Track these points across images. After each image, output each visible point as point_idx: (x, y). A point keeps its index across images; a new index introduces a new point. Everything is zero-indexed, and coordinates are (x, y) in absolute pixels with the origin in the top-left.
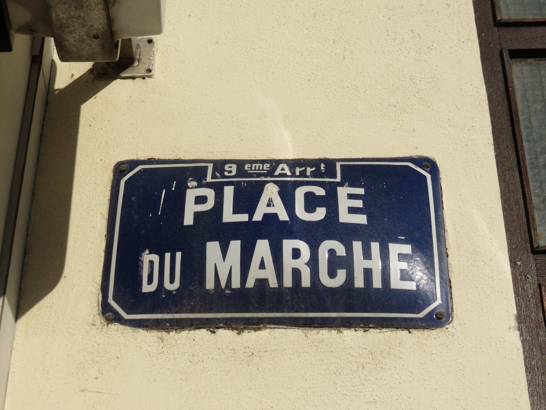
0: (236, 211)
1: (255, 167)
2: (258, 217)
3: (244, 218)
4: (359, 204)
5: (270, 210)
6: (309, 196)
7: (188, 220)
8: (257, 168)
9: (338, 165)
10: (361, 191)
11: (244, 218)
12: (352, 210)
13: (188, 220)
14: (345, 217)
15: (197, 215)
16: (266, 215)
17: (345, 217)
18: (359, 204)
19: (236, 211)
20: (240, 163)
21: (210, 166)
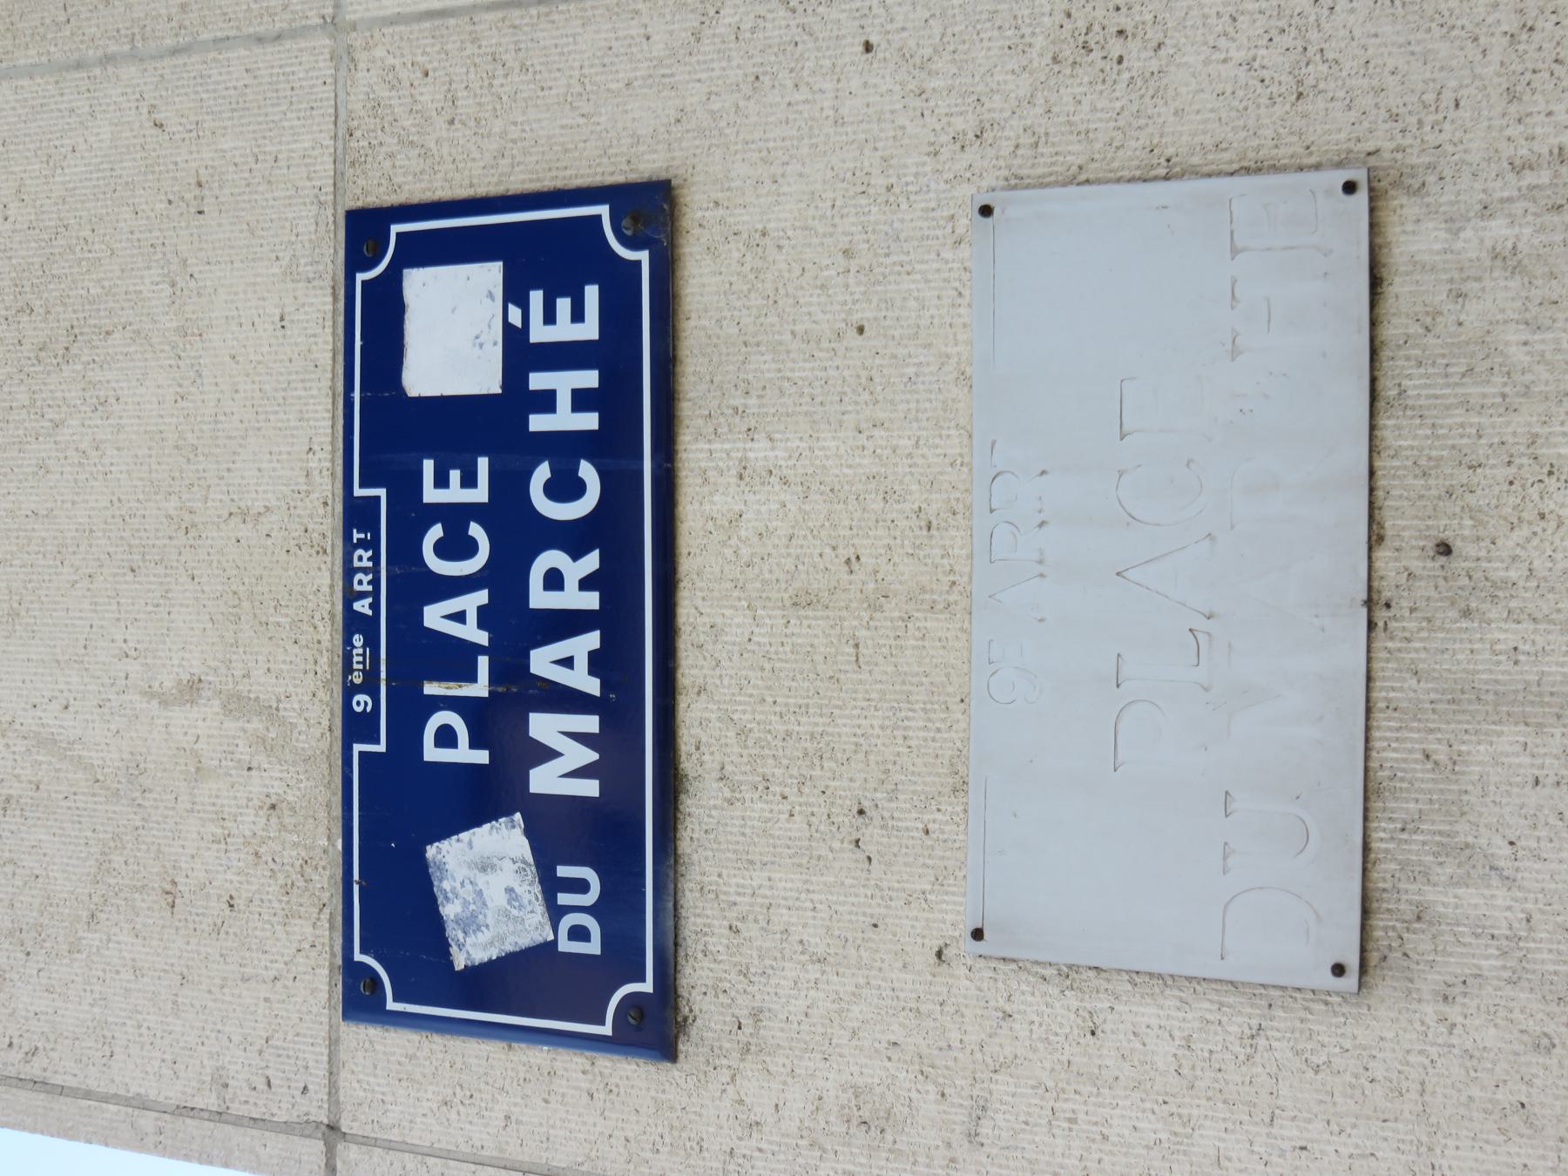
0: (472, 678)
1: (358, 663)
2: (482, 638)
3: (483, 662)
4: (564, 305)
5: (472, 617)
6: (442, 550)
7: (482, 757)
8: (361, 659)
9: (358, 492)
10: (428, 466)
11: (483, 662)
12: (578, 315)
13: (482, 757)
14: (589, 330)
15: (474, 744)
16: (481, 625)
17: (589, 330)
18: (564, 305)
19: (472, 678)
20: (349, 691)
21: (358, 748)
